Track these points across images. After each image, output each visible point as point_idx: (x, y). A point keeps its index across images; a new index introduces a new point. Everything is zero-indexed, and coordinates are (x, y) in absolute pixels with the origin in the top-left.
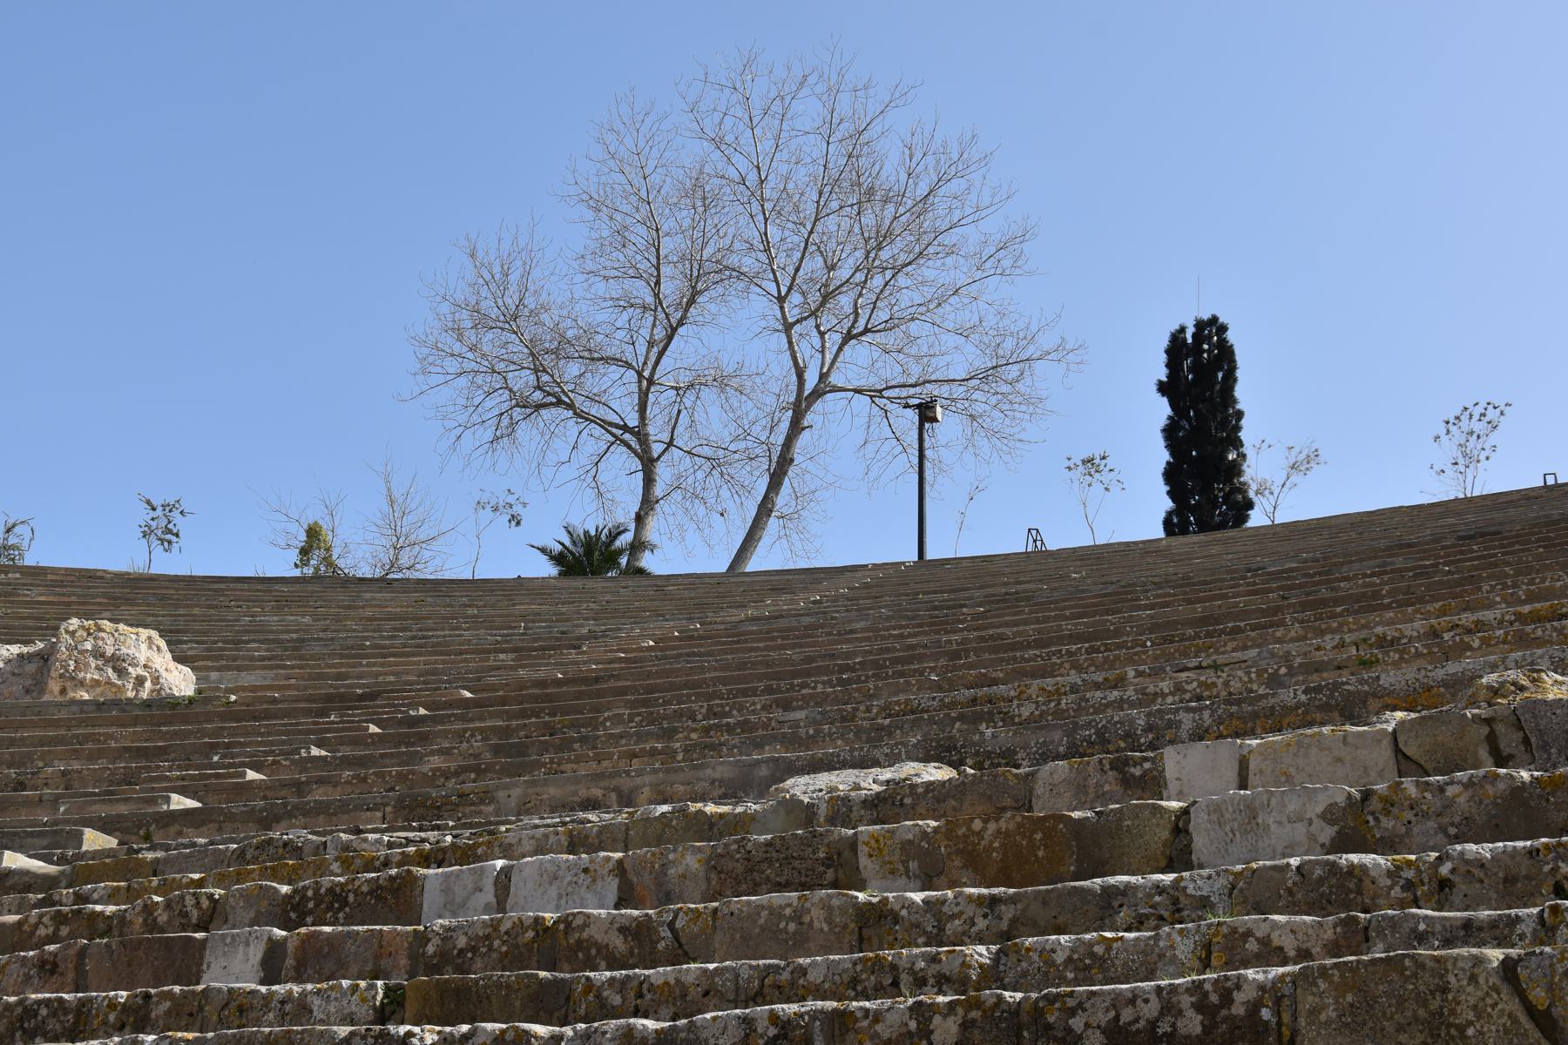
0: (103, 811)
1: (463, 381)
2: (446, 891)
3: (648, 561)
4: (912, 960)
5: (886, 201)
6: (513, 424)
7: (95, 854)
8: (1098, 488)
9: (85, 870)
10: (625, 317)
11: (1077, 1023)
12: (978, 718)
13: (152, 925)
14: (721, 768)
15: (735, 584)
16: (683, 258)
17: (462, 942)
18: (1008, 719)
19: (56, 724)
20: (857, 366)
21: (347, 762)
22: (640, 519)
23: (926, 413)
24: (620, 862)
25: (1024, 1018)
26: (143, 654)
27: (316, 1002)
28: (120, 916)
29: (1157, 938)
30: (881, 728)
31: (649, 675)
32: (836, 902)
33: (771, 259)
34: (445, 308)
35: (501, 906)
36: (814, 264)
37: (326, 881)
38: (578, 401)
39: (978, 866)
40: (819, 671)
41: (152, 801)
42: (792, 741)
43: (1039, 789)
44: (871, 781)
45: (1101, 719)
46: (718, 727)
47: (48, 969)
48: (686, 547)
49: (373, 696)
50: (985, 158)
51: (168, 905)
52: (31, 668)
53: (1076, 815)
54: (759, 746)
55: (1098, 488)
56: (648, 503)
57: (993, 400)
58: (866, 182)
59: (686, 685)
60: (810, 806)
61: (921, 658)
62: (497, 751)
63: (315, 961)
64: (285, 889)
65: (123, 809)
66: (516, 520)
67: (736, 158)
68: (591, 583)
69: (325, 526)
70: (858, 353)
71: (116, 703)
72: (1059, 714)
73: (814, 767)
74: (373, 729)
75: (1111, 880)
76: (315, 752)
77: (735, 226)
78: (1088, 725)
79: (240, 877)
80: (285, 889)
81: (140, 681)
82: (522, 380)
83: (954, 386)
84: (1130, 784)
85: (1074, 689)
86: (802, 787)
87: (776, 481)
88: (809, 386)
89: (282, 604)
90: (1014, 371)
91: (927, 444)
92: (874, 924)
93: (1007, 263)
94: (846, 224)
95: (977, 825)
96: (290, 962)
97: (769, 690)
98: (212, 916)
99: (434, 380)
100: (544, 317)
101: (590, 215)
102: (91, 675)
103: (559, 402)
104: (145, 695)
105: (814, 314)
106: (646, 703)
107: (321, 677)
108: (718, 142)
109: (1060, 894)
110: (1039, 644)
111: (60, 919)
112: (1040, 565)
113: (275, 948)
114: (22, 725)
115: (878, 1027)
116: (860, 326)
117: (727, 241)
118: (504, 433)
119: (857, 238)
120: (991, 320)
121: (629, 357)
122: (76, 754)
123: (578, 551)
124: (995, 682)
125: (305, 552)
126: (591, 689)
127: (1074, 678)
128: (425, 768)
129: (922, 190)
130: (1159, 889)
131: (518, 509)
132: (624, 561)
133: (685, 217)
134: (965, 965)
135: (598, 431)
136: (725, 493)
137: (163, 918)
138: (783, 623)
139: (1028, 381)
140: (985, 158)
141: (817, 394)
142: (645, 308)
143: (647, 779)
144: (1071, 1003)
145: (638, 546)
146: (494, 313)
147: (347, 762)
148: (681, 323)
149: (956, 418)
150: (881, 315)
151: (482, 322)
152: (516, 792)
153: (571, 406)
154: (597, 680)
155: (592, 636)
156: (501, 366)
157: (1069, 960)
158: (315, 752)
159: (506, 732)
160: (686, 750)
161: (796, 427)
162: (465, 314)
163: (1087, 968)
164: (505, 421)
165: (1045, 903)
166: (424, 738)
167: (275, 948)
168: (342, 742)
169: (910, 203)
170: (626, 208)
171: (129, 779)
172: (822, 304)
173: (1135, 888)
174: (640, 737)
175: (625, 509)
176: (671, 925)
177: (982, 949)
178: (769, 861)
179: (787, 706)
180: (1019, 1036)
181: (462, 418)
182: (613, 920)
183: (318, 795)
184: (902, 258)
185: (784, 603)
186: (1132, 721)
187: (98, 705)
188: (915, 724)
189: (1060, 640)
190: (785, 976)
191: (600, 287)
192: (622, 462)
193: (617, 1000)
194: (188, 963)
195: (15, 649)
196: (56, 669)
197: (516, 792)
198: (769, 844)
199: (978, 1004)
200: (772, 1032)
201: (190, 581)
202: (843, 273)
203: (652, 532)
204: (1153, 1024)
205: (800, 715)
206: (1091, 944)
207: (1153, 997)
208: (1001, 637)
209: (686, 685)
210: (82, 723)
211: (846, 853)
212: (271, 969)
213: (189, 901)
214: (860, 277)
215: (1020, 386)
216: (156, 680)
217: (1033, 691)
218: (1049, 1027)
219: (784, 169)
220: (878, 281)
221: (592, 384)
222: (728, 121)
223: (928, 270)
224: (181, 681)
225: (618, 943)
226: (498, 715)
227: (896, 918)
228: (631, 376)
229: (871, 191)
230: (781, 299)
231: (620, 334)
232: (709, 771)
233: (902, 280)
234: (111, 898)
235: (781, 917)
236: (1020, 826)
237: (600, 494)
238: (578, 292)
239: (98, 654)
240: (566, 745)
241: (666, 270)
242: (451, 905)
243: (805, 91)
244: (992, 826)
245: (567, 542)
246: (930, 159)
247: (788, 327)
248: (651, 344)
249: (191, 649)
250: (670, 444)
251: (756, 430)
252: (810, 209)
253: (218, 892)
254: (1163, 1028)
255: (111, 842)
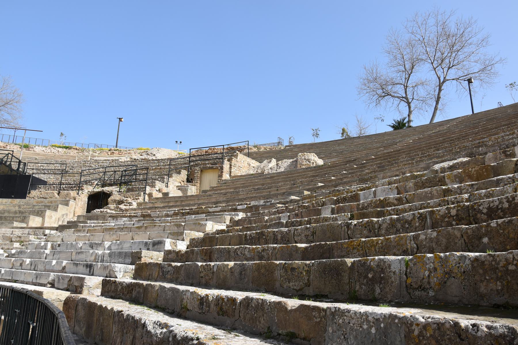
0: (307, 187)
1: (367, 94)
2: (364, 196)
3: (412, 124)
4: (451, 199)
5: (453, 36)
6: (379, 101)
7: (306, 195)
8: (514, 90)
9: (304, 198)
10: (399, 74)
11: (481, 208)
12: (479, 147)
13: (314, 207)
14: (422, 165)
15: (432, 125)
16: (409, 59)
17: (366, 205)
18: (486, 145)
19: (299, 173)
20: (452, 73)
21: (350, 173)
22: (409, 116)
23: (470, 81)
24: (397, 186)
25: (470, 208)
26: (313, 158)
27: (338, 218)
28: (309, 205)
29: (504, 188)
30: (458, 152)
31: (410, 148)
32: (438, 189)
33: (429, 55)
34: (361, 80)
35: (375, 197)
36: (439, 54)
37: (342, 196)
38: (392, 94)
39: (471, 178)
40: (446, 142)
41: (315, 185)
42: (438, 157)
43: (486, 160)
44: (451, 163)
45: (507, 143)
46: (423, 157)
47: (297, 215)
48: (420, 119)
49: (355, 160)
50: (475, 22)
51: (316, 203)
52: (294, 163)
53: (492, 164)
54: (431, 159)
55: (514, 90)
56: (410, 112)
57: (486, 75)
58: (448, 34)
59: (417, 149)
60: (437, 170)
61: (469, 135)
62: (379, 167)
63: (339, 210)
64: (335, 198)
65: (311, 187)
66: (383, 120)
67: (417, 35)
68: (400, 131)
69: (346, 129)
70: (452, 71)
71: (309, 168)
72: (498, 143)
73: (437, 163)
74: (355, 166)
75: (498, 177)
76: (344, 172)
77: (420, 49)
78: (504, 144)
79: (329, 197)
80: (335, 198)
81: (313, 163)
82: (380, 92)
83: (475, 74)
84: (507, 156)
85: (502, 137)
86: (437, 167)
87: (437, 102)
88: (442, 81)
89: (339, 145)
90: (490, 68)
91: (471, 88)
92: (448, 192)
93: (484, 44)
94: (444, 43)
95: (470, 169)
96: (336, 211)
97: (435, 147)
98: (324, 204)
99: (362, 95)
100: (382, 78)
101: (388, 55)
102: (304, 163)
103: (388, 95)
104: (314, 166)
105: (440, 64)
106: (409, 154)
107: (346, 158)
108: (412, 33)
109: (487, 182)
110: (496, 128)
111: (299, 207)
112: (502, 110)
113: (333, 209)
114: (294, 174)
115: (440, 213)
116: (451, 65)
117: (418, 54)
118: (378, 103)
119: (448, 46)
120: (482, 58)
121: (401, 82)
122: (303, 178)
123: (397, 124)
124: (484, 138)
125: (342, 134)
126: (398, 152)
127: (503, 134)
128: (364, 173)
129: (461, 32)
130: (510, 178)
131: (383, 118)
132: (407, 125)
133: (408, 50)
134: (462, 199)
135: (397, 99)
136: (427, 107)
137: (315, 205)
138: (440, 133)
139: (493, 69)
140: (475, 22)
141: (444, 82)
142: (403, 71)
143: (408, 169)
144: (479, 204)
145: (409, 121)
146: (372, 79)
147: (350, 173)
148: (411, 73)
149: (477, 81)
150: (456, 62)
151: (369, 82)
152: (381, 175)
153: (391, 95)
154: (399, 150)
155: (400, 141)
156: (375, 90)
157: (485, 195)
158: (344, 172)
159: (381, 163)
160: (416, 162)
161: (440, 90)
162: (366, 81)
163: (489, 196)
164: (378, 100)
165: (484, 184)
166: (365, 167)
167: (333, 209)
168: (349, 170)
169: (459, 36)
170: (396, 51)
171: (312, 181)
172: (442, 62)
173: (504, 178)
174: (407, 161)
175: (406, 114)
176: (405, 197)
177: (466, 195)
178: (427, 182)
179: (438, 150)
180: (469, 211)
181: (369, 102)
182: (394, 198)
183: (345, 180)
184: (459, 48)
185: (441, 128)
186: (514, 142)
187: (306, 168)
188: (465, 150)
189: (501, 126)
190: (426, 205)
191: (393, 69)
192: (404, 105)
193: (393, 213)
194: (319, 212)
195: (291, 160)
196: (298, 163)
197: (381, 175)
198: (426, 179)
199: (460, 206)
200: (419, 216)
201: (323, 143)
202: (446, 55)
203: (412, 118)
204: (497, 206)
205: (441, 151)
206: (489, 191)
207: (497, 201)
208: (487, 128)
209: (417, 149)
210: (304, 172)
211: (443, 179)
212: (333, 212)
213: (319, 202)
214: (449, 55)
215: (492, 71)
216: (316, 162)
217: (493, 139)
218: (475, 209)
219: (428, 35)
220: (454, 55)
221: (394, 89)
222: (414, 28)
223: (465, 50)
224: (320, 162)
225: (395, 202)
226: (379, 160)
227: (451, 191)
228: (402, 86)
229: (449, 35)
230: (432, 63)
231: (399, 78)
232: (420, 166)
233: (459, 53)
234: (308, 202)
235: (427, 193)
236: (480, 168)
237: (400, 112)
238: (388, 71)
239: (305, 159)
240: (392, 164)
241: (406, 63)
242: (365, 197)
243: (430, 17)
244: (473, 169)
245: (394, 123)
246: (462, 25)
247: (435, 69)
248: (406, 79)
249: (323, 156)
250: (413, 99)
251: (431, 92)
252: (436, 42)
253: (324, 200)
254: (500, 207)
255: (309, 193)
